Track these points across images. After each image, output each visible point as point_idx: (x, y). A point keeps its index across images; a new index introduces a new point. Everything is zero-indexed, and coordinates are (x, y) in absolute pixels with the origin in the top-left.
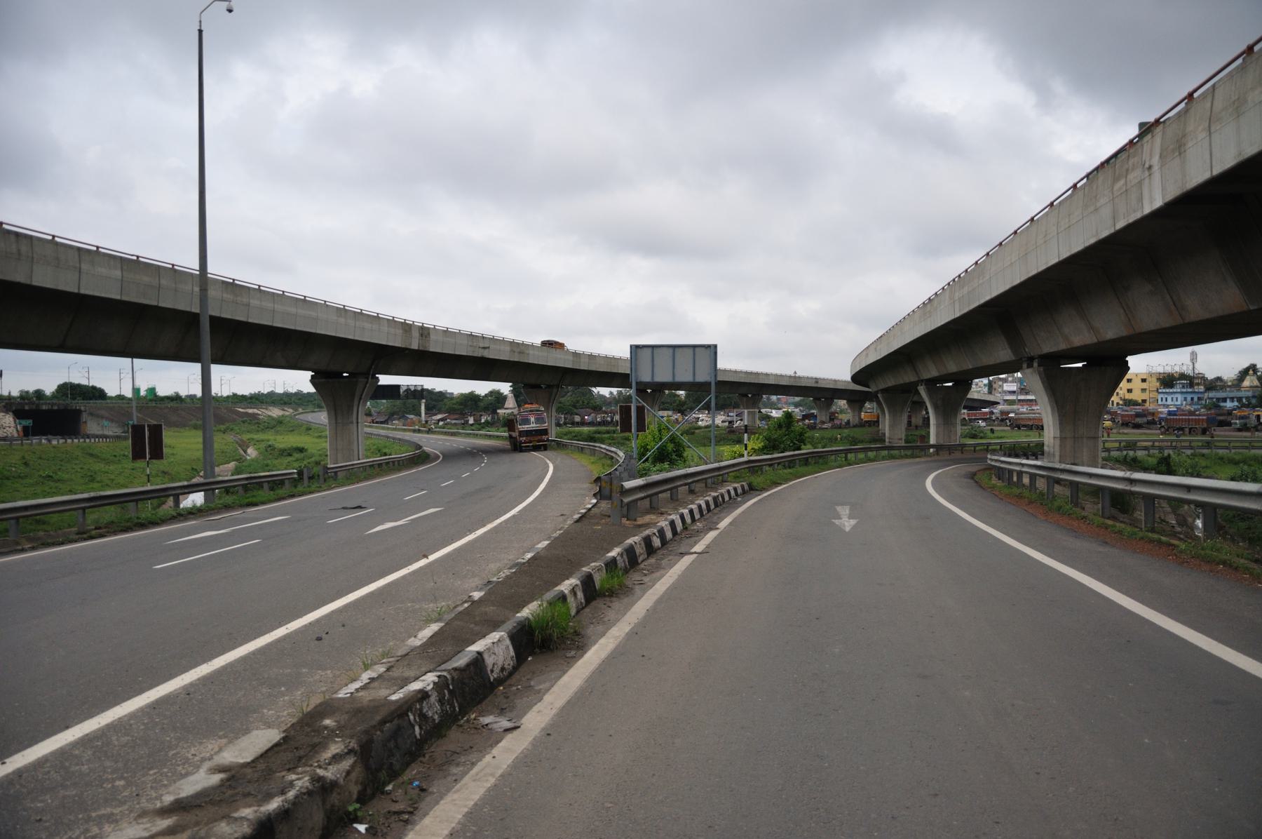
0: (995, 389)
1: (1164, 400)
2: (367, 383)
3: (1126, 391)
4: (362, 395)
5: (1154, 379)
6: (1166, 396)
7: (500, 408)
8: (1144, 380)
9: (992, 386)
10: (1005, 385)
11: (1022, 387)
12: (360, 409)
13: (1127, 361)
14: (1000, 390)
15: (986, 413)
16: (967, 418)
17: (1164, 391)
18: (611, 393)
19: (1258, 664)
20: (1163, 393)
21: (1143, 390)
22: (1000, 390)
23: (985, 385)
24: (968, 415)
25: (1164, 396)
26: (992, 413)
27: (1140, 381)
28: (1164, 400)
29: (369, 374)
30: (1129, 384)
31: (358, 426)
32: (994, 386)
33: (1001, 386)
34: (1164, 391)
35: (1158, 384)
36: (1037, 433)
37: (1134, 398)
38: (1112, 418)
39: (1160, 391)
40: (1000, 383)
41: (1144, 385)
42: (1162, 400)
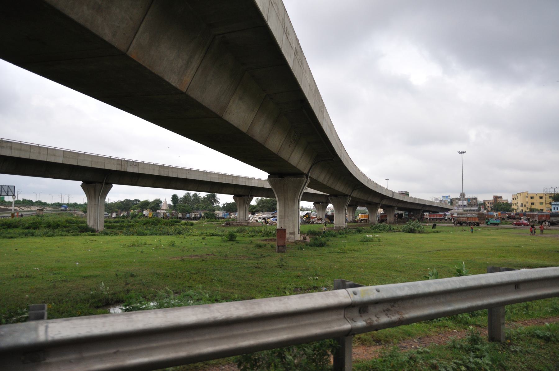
0: (454, 204)
1: (556, 209)
2: (102, 187)
3: (531, 204)
4: (98, 205)
5: (548, 196)
6: (557, 206)
7: (158, 209)
8: (541, 198)
9: (452, 203)
10: (459, 201)
11: (469, 203)
12: (146, 17)
13: (112, 186)
14: (457, 205)
15: (442, 215)
16: (428, 218)
17: (555, 203)
18: (175, 198)
19: (2, 154)
20: (554, 204)
21: (541, 203)
22: (457, 205)
23: (448, 202)
24: (430, 216)
25: (556, 207)
26: (445, 215)
27: (539, 198)
28: (556, 209)
29: (103, 182)
30: (541, 199)
31: (98, 207)
32: (454, 202)
33: (457, 203)
34: (555, 203)
35: (551, 199)
36: (470, 228)
37: (536, 208)
38: (527, 219)
39: (553, 203)
40: (457, 201)
41: (542, 201)
42: (554, 209)
